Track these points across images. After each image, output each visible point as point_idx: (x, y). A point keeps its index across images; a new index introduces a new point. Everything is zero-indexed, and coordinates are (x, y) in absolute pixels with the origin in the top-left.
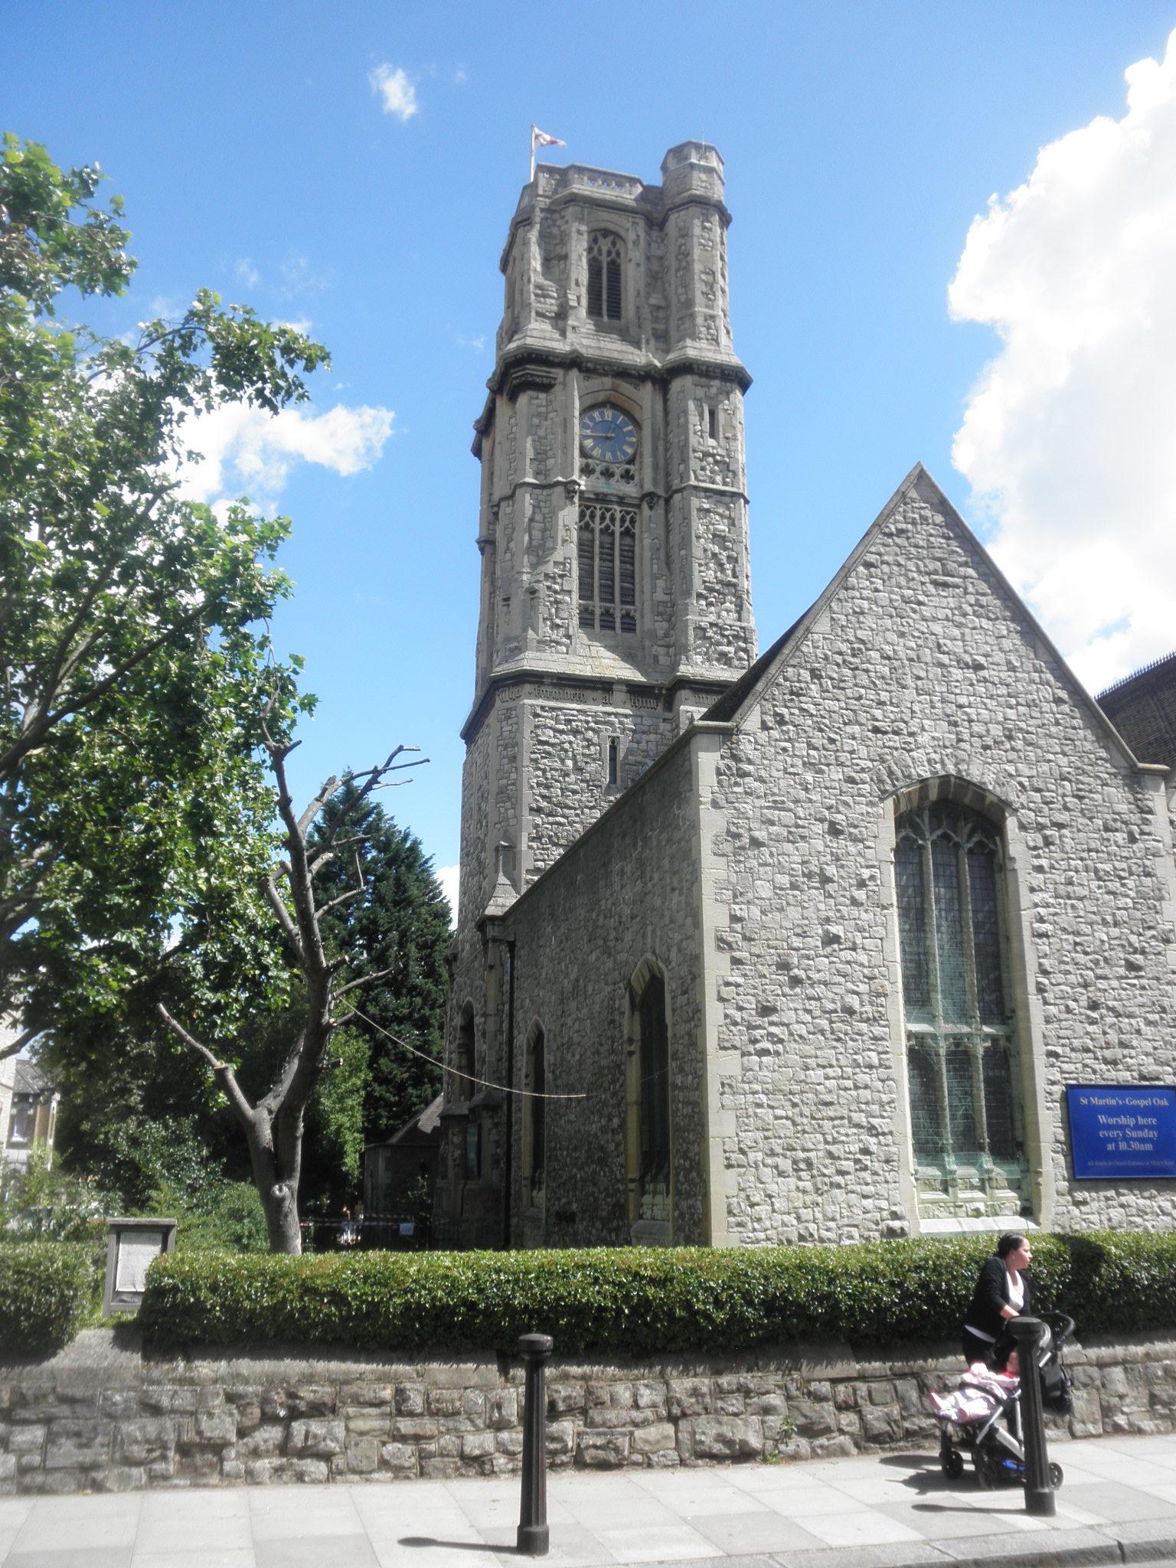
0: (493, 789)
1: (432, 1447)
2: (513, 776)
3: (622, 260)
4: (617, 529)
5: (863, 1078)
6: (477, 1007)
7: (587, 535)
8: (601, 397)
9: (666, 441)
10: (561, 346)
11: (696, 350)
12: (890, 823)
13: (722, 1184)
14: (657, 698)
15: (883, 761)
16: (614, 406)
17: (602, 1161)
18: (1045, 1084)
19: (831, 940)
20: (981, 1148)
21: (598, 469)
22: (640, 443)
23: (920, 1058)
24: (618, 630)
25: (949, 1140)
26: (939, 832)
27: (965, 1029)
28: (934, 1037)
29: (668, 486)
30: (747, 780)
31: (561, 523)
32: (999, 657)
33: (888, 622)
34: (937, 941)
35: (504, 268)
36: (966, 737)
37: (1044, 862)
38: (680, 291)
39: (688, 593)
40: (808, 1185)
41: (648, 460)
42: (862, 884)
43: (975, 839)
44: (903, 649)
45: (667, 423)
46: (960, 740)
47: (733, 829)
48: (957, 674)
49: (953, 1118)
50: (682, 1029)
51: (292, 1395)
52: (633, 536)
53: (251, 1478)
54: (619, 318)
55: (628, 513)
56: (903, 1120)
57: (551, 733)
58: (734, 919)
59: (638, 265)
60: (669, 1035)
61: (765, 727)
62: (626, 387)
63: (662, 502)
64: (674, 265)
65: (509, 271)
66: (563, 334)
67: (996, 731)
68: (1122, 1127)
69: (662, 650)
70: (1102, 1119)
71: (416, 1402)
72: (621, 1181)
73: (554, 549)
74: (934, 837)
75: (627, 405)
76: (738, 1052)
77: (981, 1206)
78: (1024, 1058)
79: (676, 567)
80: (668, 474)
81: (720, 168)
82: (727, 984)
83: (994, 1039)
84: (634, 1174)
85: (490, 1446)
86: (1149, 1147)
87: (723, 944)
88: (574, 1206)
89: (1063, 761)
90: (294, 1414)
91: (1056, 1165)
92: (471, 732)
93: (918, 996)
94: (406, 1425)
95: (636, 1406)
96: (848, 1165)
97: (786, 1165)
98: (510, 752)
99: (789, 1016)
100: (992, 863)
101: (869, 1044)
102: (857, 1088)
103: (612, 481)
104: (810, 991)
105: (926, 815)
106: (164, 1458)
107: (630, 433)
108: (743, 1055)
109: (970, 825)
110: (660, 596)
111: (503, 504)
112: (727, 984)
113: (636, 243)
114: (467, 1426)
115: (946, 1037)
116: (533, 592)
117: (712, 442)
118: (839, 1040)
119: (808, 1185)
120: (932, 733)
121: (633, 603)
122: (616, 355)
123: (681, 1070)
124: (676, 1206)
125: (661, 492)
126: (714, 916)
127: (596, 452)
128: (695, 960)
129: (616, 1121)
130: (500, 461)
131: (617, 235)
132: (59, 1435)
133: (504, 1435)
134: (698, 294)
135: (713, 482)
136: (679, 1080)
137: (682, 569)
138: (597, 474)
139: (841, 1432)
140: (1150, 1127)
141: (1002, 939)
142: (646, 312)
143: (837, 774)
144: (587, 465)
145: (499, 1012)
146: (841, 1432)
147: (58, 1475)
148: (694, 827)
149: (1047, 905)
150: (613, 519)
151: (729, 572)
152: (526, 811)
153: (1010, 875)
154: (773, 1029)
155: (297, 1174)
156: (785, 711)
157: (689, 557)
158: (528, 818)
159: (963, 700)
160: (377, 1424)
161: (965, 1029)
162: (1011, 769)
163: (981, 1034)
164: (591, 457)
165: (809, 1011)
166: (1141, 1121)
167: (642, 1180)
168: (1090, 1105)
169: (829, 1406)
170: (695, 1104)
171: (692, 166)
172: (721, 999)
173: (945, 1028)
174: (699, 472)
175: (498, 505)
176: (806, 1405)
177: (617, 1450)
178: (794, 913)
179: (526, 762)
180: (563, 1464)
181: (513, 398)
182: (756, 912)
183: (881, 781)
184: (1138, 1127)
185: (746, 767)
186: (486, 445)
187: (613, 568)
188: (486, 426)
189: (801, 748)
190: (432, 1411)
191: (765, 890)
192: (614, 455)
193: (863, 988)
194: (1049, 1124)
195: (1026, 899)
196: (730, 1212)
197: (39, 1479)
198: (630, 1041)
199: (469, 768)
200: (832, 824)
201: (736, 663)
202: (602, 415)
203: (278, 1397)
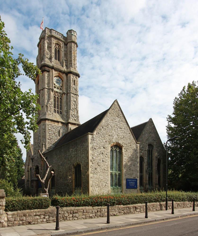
1: (87, 216)
2: (45, 134)
4: (59, 98)
5: (106, 177)
8: (57, 75)
10: (51, 65)
11: (72, 70)
13: (91, 189)
14: (65, 124)
15: (110, 140)
18: (124, 178)
19: (103, 161)
21: (57, 87)
23: (111, 174)
24: (59, 114)
26: (115, 149)
27: (116, 172)
28: (113, 173)
29: (67, 92)
30: (94, 141)
31: (51, 96)
33: (111, 121)
34: (114, 162)
36: (119, 137)
37: (126, 153)
38: (70, 58)
39: (70, 110)
40: (100, 189)
42: (107, 155)
44: (113, 125)
46: (118, 138)
47: (93, 147)
48: (119, 129)
51: (73, 211)
52: (61, 99)
53: (70, 220)
55: (61, 95)
57: (50, 128)
58: (93, 158)
59: (63, 52)
61: (97, 134)
62: (61, 74)
63: (66, 94)
64: (69, 53)
65: (39, 47)
66: (51, 62)
67: (122, 137)
68: (132, 183)
70: (130, 182)
71: (85, 212)
73: (50, 100)
75: (61, 77)
78: (122, 175)
79: (68, 105)
81: (76, 36)
83: (119, 173)
84: (74, 187)
85: (92, 215)
88: (62, 191)
89: (129, 141)
90: (73, 213)
91: (125, 187)
93: (112, 168)
94: (84, 214)
95: (105, 211)
96: (104, 187)
97: (97, 187)
98: (44, 130)
99: (98, 170)
100: (121, 153)
101: (107, 173)
102: (105, 178)
106: (61, 218)
107: (61, 82)
111: (41, 91)
113: (63, 47)
114: (90, 214)
116: (47, 106)
117: (74, 86)
118: (103, 173)
119: (100, 189)
120: (115, 137)
121: (61, 110)
122: (59, 68)
126: (90, 158)
128: (88, 164)
132: (50, 217)
133: (93, 214)
134: (73, 59)
135: (74, 92)
136: (84, 177)
137: (69, 106)
138: (59, 89)
139: (122, 213)
140: (134, 183)
143: (104, 141)
144: (55, 86)
146: (122, 213)
147: (51, 221)
148: (88, 146)
151: (76, 107)
152: (47, 139)
153: (122, 155)
154: (96, 171)
155: (48, 188)
156: (99, 132)
157: (70, 104)
158: (47, 140)
159: (119, 133)
160: (81, 214)
161: (116, 172)
162: (123, 142)
163: (118, 172)
164: (55, 85)
167: (75, 188)
168: (129, 181)
169: (121, 210)
171: (72, 34)
172: (91, 168)
174: (72, 90)
175: (40, 91)
176: (119, 210)
177: (103, 215)
178: (99, 158)
179: (47, 132)
180: (99, 217)
182: (95, 157)
183: (109, 142)
184: (133, 183)
185: (94, 139)
187: (58, 104)
189: (101, 137)
190: (86, 212)
191: (96, 155)
193: (106, 167)
194: (124, 182)
195: (124, 157)
197: (49, 221)
198: (73, 172)
201: (76, 121)
203: (72, 212)
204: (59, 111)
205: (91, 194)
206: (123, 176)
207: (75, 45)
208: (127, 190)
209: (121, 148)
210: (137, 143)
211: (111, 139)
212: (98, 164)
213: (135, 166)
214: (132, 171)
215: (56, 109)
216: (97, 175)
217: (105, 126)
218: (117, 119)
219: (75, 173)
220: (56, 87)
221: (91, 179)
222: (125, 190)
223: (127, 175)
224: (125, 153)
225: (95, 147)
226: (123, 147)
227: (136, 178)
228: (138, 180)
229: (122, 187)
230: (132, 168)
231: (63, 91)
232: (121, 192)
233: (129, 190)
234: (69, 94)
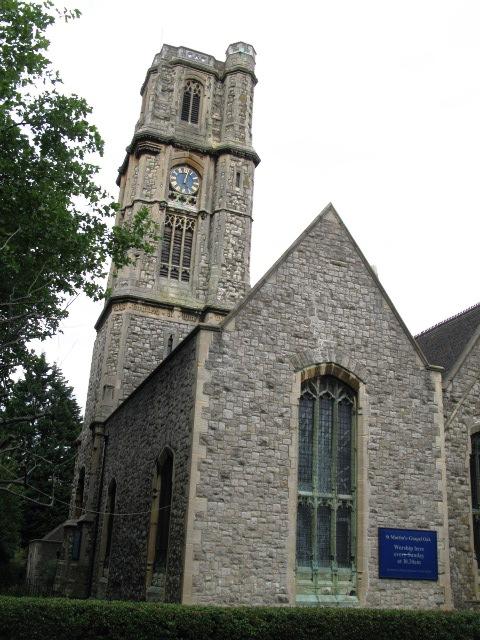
0: (106, 356)
3: (201, 95)
4: (185, 228)
6: (86, 470)
7: (168, 230)
8: (183, 161)
9: (215, 187)
12: (298, 384)
13: (191, 568)
14: (196, 315)
16: (189, 166)
17: (136, 555)
20: (331, 558)
22: (201, 186)
23: (303, 508)
25: (315, 552)
26: (324, 392)
27: (330, 495)
28: (312, 498)
29: (213, 208)
32: (362, 304)
35: (142, 93)
36: (342, 344)
41: (204, 195)
42: (281, 416)
43: (343, 397)
45: (215, 177)
48: (340, 311)
49: (319, 542)
50: (179, 485)
52: (192, 232)
54: (196, 123)
56: (290, 541)
60: (173, 488)
62: (196, 157)
63: (208, 217)
68: (407, 552)
69: (202, 292)
70: (396, 547)
72: (144, 564)
74: (321, 394)
76: (206, 499)
77: (329, 589)
80: (213, 203)
82: (204, 462)
86: (418, 563)
87: (204, 440)
92: (99, 326)
93: (305, 477)
96: (261, 563)
97: (227, 560)
99: (235, 482)
100: (350, 409)
103: (185, 204)
104: (248, 470)
105: (318, 382)
107: (196, 181)
108: (209, 500)
109: (340, 390)
110: (203, 264)
112: (204, 462)
115: (319, 498)
121: (188, 266)
123: (176, 507)
124: (168, 579)
125: (209, 211)
126: (200, 425)
127: (178, 188)
128: (188, 448)
129: (144, 533)
130: (128, 189)
131: (199, 82)
136: (175, 511)
140: (421, 553)
141: (353, 450)
142: (210, 121)
143: (273, 357)
145: (97, 473)
148: (194, 378)
149: (377, 434)
150: (183, 223)
162: (364, 362)
165: (246, 480)
166: (416, 549)
170: (182, 525)
173: (316, 494)
175: (124, 210)
178: (243, 428)
181: (138, 157)
184: (415, 552)
186: (122, 180)
188: (123, 171)
189: (255, 342)
192: (187, 191)
196: (194, 585)
199: (97, 342)
200: (268, 383)
202: (182, 170)
204: (181, 268)
205: (190, 599)
206: (362, 518)
207: (249, 79)
208: (382, 584)
209: (352, 389)
210: (429, 369)
211: (305, 349)
212: (236, 456)
213: (422, 470)
214: (410, 493)
215: (170, 264)
216: (227, 505)
217: (279, 297)
218: (335, 274)
219: (161, 495)
220: (175, 198)
221: (199, 524)
222: (372, 585)
223: (384, 513)
224: (373, 411)
225: (227, 380)
226: (361, 384)
227: (432, 528)
228: (440, 536)
229: (356, 567)
230: (408, 477)
231: (199, 208)
232: (352, 593)
233: (395, 583)
234: (217, 214)
